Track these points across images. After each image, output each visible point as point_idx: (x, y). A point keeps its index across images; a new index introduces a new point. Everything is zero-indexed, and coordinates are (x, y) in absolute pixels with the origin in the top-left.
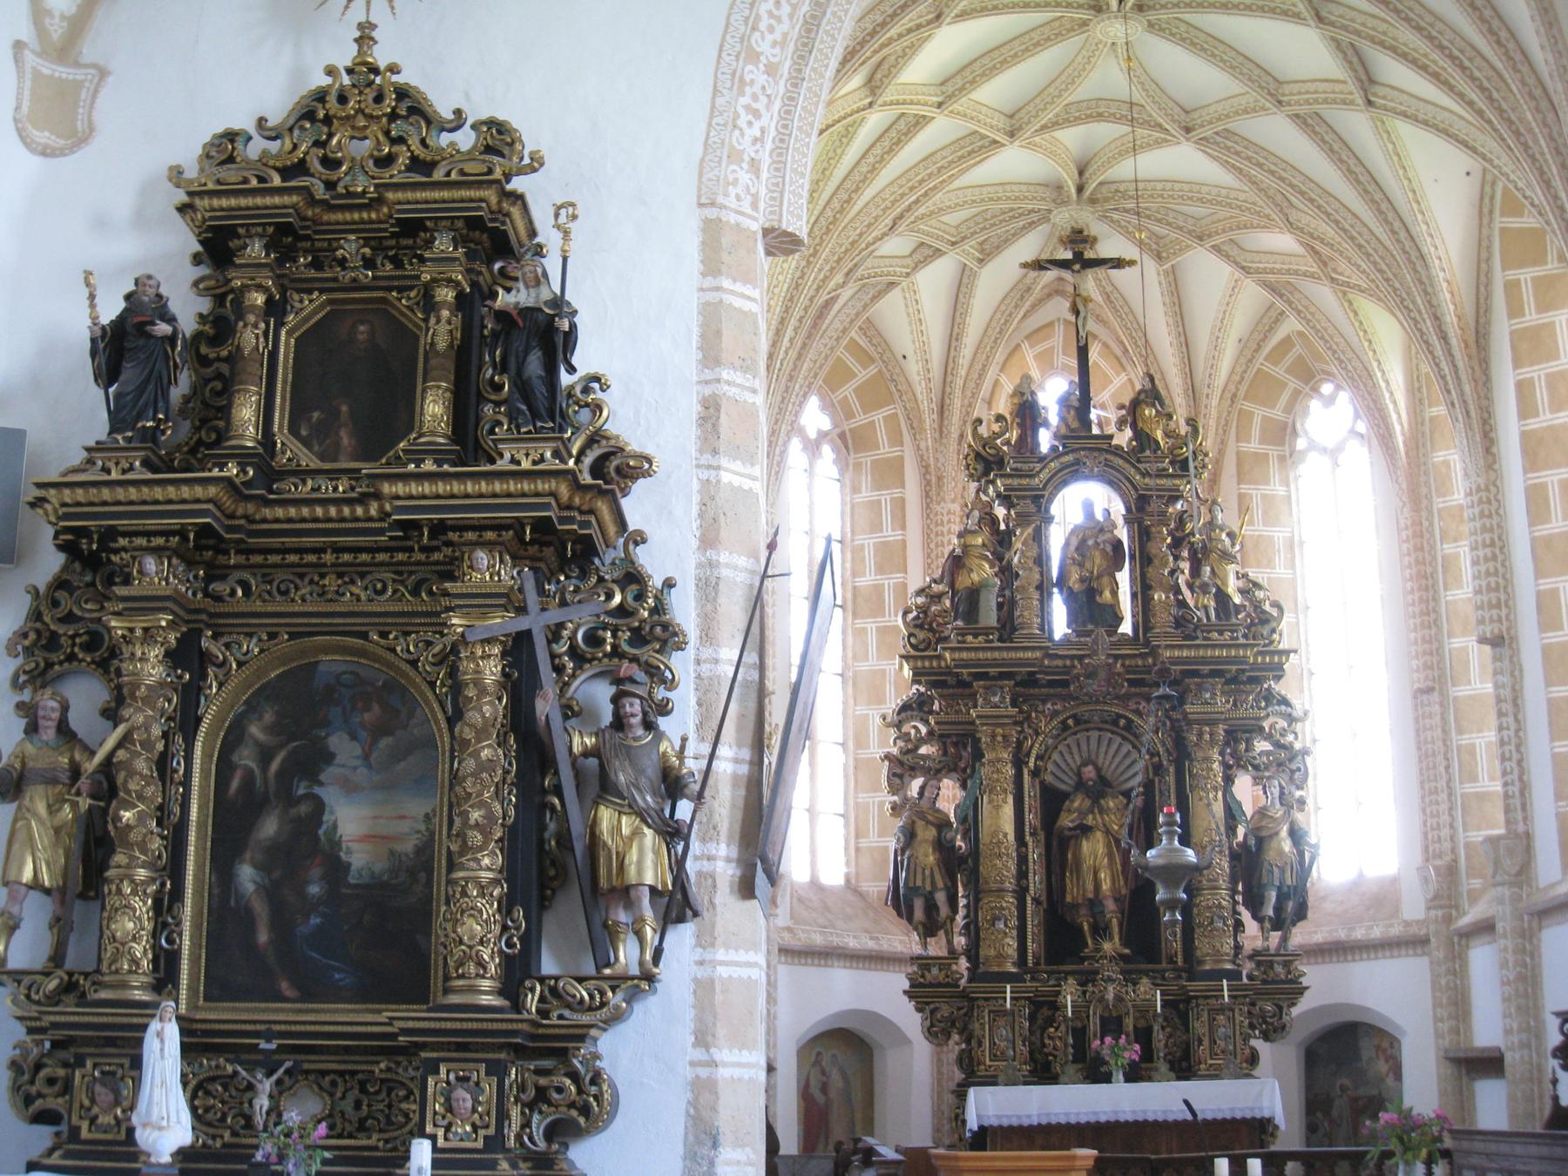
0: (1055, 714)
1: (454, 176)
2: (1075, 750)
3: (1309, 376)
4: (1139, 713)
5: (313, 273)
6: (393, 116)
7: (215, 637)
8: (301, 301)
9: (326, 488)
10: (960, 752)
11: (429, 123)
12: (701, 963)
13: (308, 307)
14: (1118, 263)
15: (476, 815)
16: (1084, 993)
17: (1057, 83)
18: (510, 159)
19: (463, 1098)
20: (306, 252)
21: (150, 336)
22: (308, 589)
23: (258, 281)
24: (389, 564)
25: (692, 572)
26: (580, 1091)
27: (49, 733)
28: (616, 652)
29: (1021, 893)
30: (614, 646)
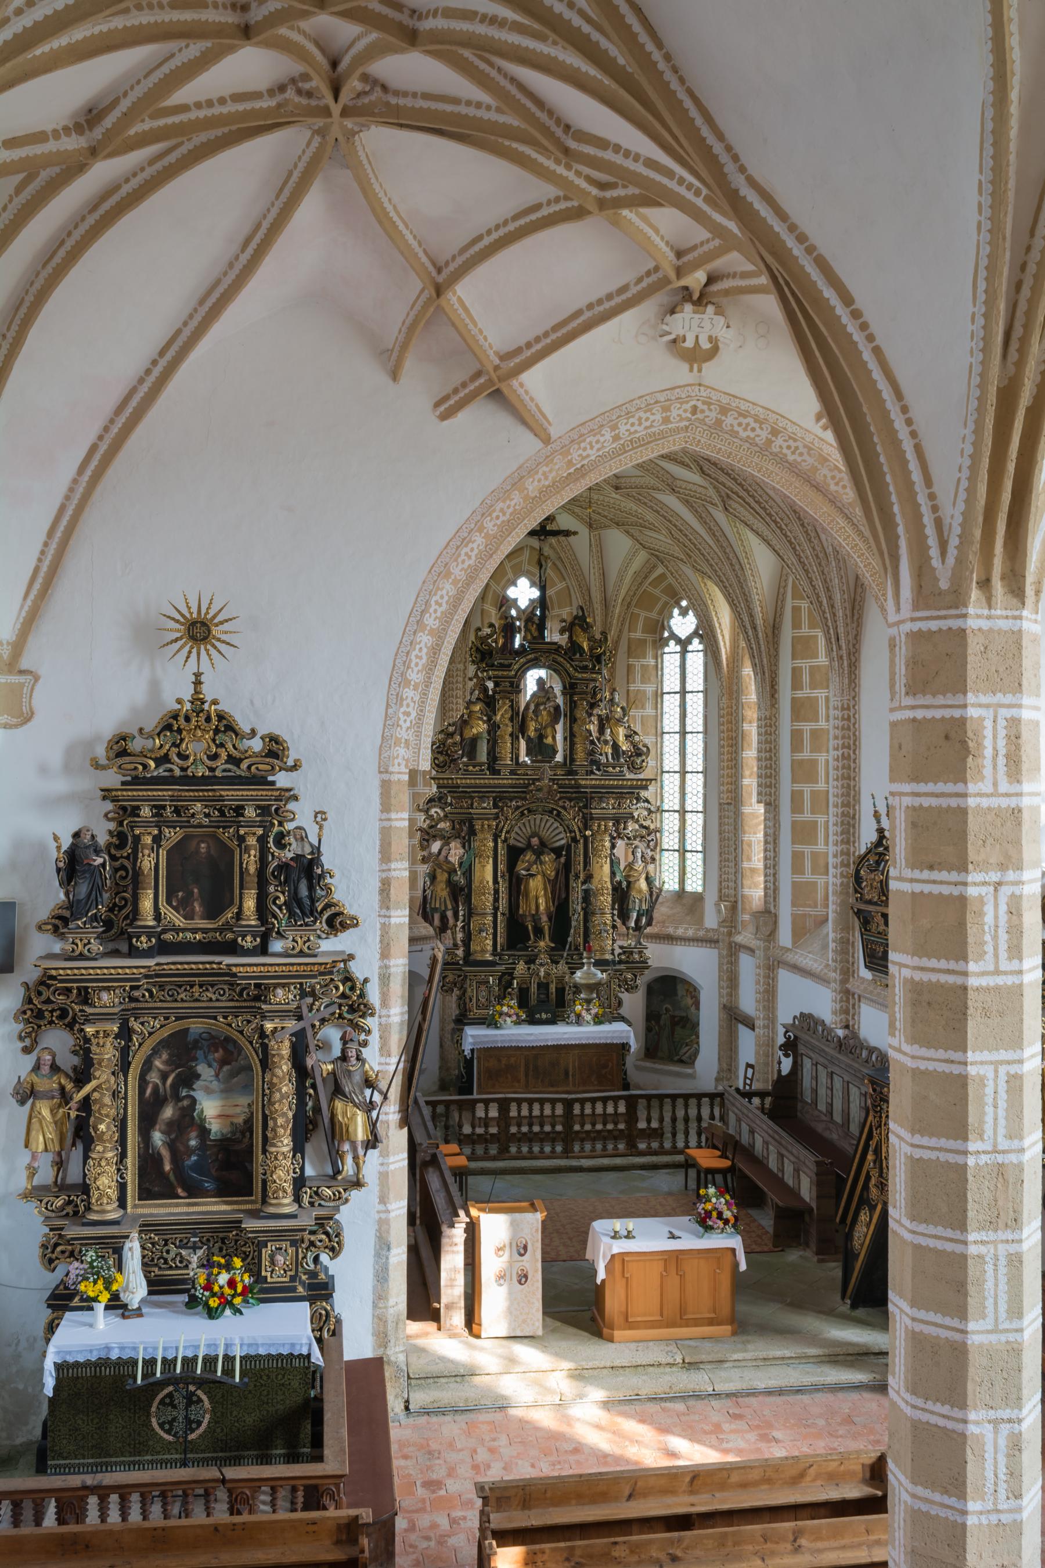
0: (518, 808)
3: (674, 597)
4: (564, 808)
10: (465, 830)
11: (237, 735)
13: (172, 836)
19: (280, 1259)
25: (376, 971)
29: (496, 909)
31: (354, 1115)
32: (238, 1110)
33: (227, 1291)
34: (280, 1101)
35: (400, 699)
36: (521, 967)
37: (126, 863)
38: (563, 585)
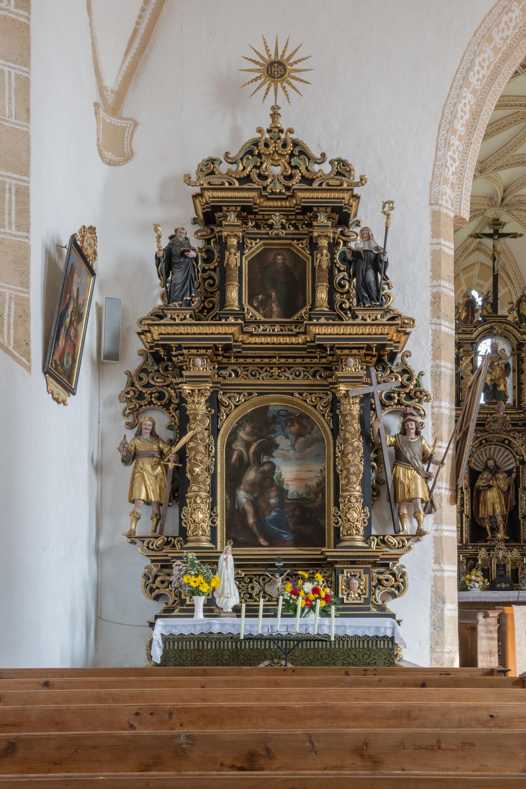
1: (324, 186)
2: (484, 453)
4: (514, 438)
5: (256, 231)
6: (292, 155)
7: (224, 394)
8: (251, 244)
9: (269, 329)
11: (309, 159)
12: (436, 530)
13: (255, 247)
14: (514, 236)
15: (352, 470)
16: (489, 554)
17: (507, 146)
18: (349, 178)
19: (355, 582)
20: (252, 220)
21: (186, 257)
22: (265, 374)
23: (235, 233)
24: (301, 364)
26: (396, 581)
27: (146, 435)
28: (399, 403)
30: (399, 400)
31: (414, 479)
32: (312, 475)
33: (312, 597)
34: (352, 453)
35: (448, 145)
36: (483, 553)
37: (213, 274)
38: (507, 289)
